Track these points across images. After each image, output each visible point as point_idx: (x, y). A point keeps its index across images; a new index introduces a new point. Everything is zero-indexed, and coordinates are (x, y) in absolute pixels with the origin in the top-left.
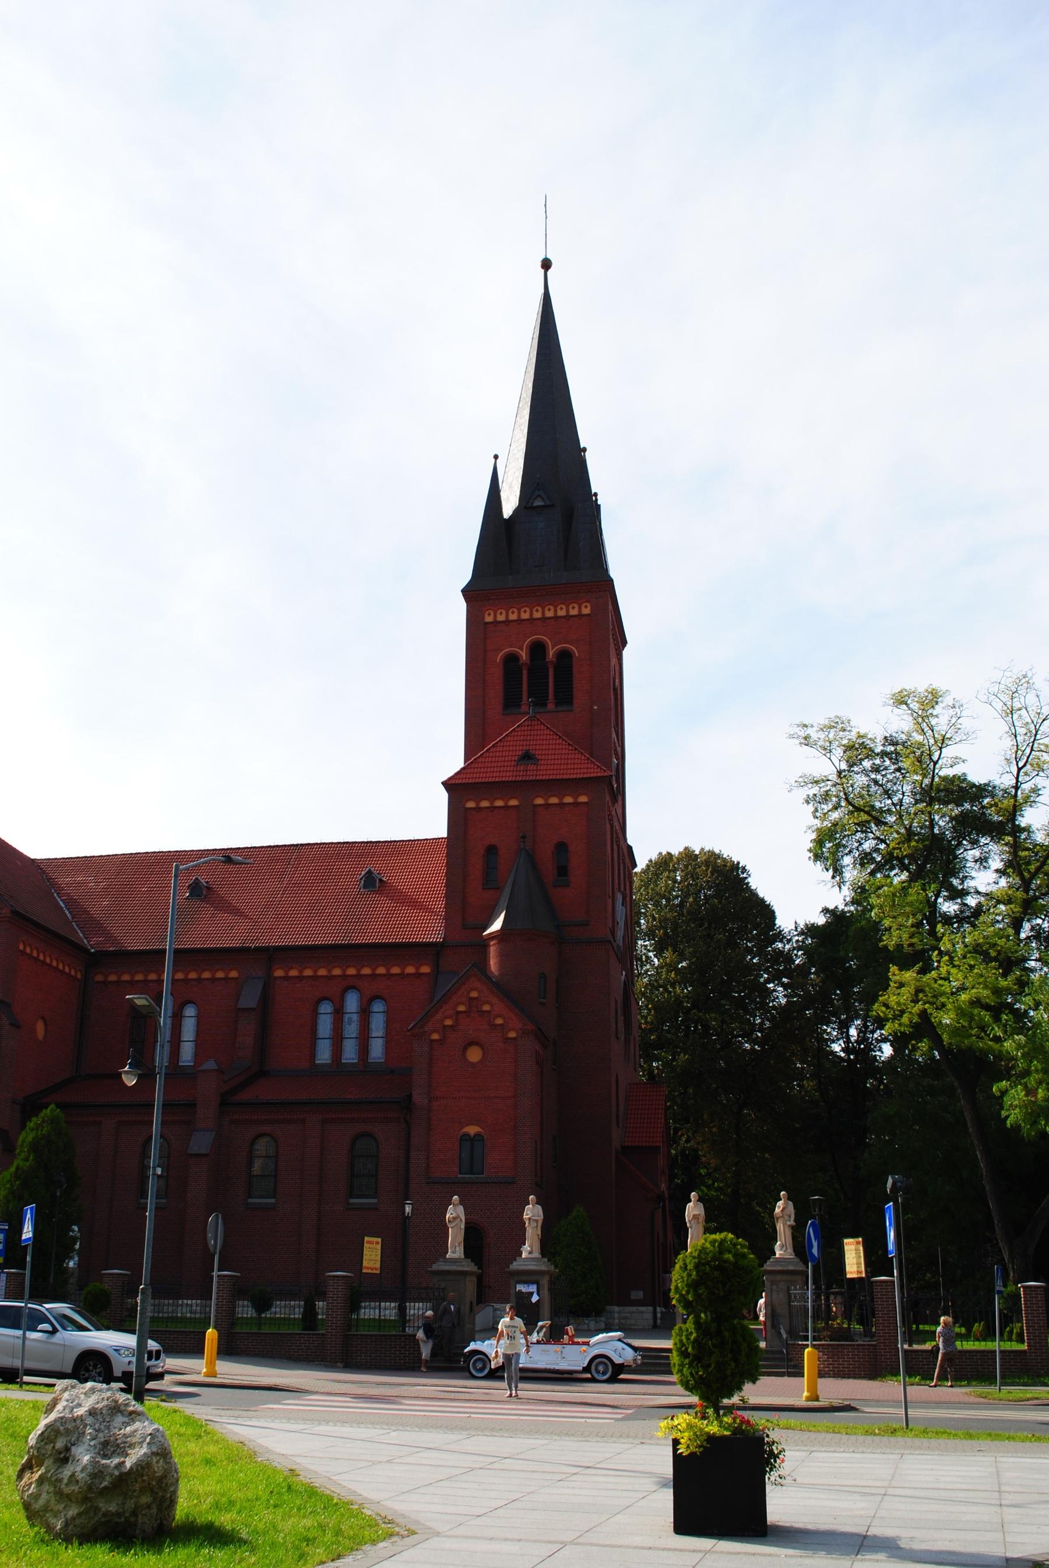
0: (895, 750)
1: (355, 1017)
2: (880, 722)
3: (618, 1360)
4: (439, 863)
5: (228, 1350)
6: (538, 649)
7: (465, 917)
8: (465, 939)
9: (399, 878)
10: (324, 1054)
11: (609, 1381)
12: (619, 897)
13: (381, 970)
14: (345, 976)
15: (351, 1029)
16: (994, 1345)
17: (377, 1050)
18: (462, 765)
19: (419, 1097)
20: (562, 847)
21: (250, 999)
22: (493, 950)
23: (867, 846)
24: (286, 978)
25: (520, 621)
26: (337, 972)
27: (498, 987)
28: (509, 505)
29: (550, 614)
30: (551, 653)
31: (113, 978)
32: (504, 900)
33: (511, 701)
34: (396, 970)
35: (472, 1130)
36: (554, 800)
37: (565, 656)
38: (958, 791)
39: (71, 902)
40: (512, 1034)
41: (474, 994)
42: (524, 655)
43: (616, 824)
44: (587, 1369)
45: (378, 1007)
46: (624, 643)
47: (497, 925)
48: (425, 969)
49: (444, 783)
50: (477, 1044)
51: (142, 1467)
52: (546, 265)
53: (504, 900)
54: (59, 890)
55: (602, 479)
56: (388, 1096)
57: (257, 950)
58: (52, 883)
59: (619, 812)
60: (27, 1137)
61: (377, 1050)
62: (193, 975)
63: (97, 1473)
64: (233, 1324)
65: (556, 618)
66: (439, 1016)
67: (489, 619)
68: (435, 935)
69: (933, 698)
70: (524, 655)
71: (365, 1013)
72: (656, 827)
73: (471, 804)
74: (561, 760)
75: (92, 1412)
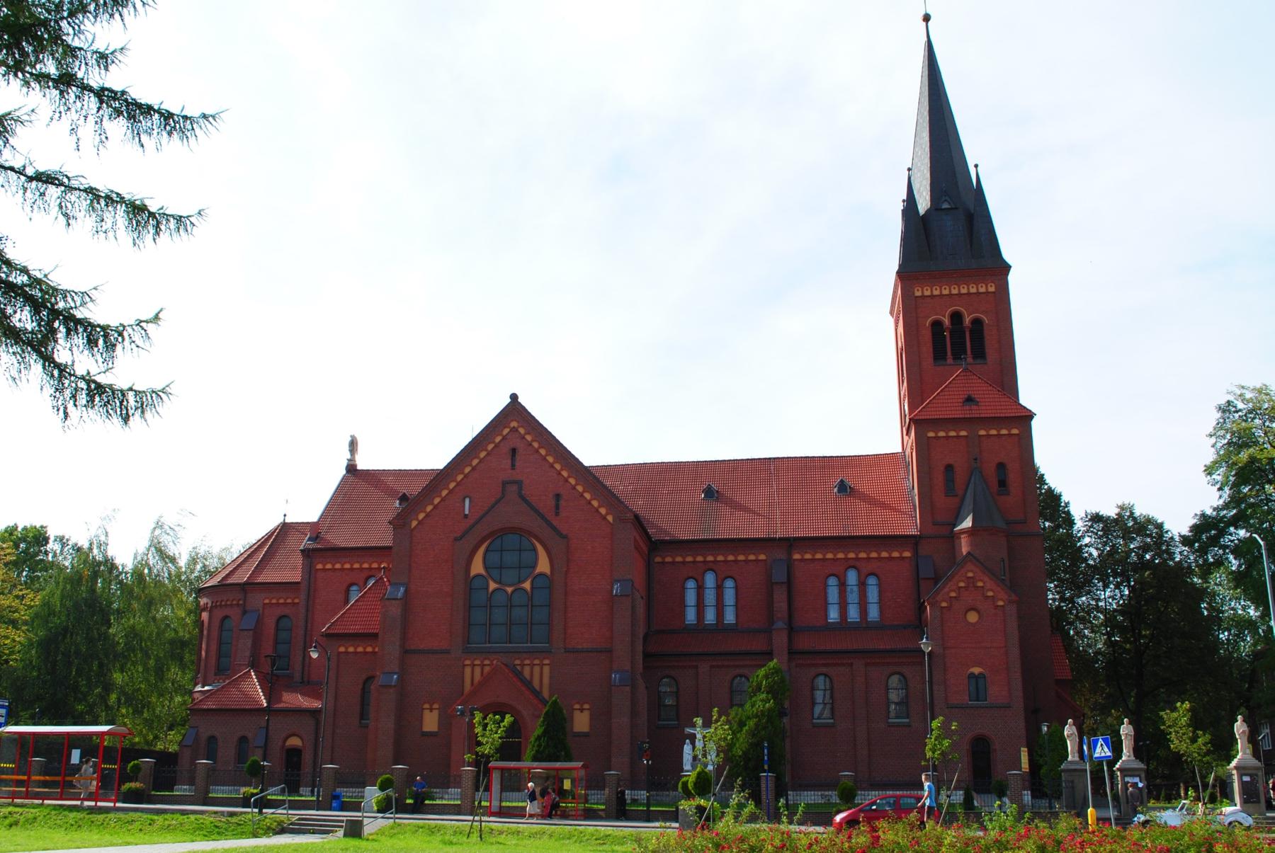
1: (855, 589)
6: (956, 317)
13: (874, 555)
14: (847, 559)
17: (730, 617)
20: (1001, 466)
21: (780, 575)
24: (802, 560)
25: (941, 295)
26: (841, 556)
28: (923, 204)
29: (964, 291)
30: (967, 320)
31: (669, 559)
33: (939, 355)
35: (976, 670)
36: (994, 432)
37: (977, 322)
40: (1001, 603)
41: (970, 575)
42: (946, 321)
47: (967, 523)
48: (907, 554)
49: (514, 411)
52: (927, 18)
57: (780, 539)
61: (874, 613)
65: (969, 294)
66: (946, 590)
67: (918, 294)
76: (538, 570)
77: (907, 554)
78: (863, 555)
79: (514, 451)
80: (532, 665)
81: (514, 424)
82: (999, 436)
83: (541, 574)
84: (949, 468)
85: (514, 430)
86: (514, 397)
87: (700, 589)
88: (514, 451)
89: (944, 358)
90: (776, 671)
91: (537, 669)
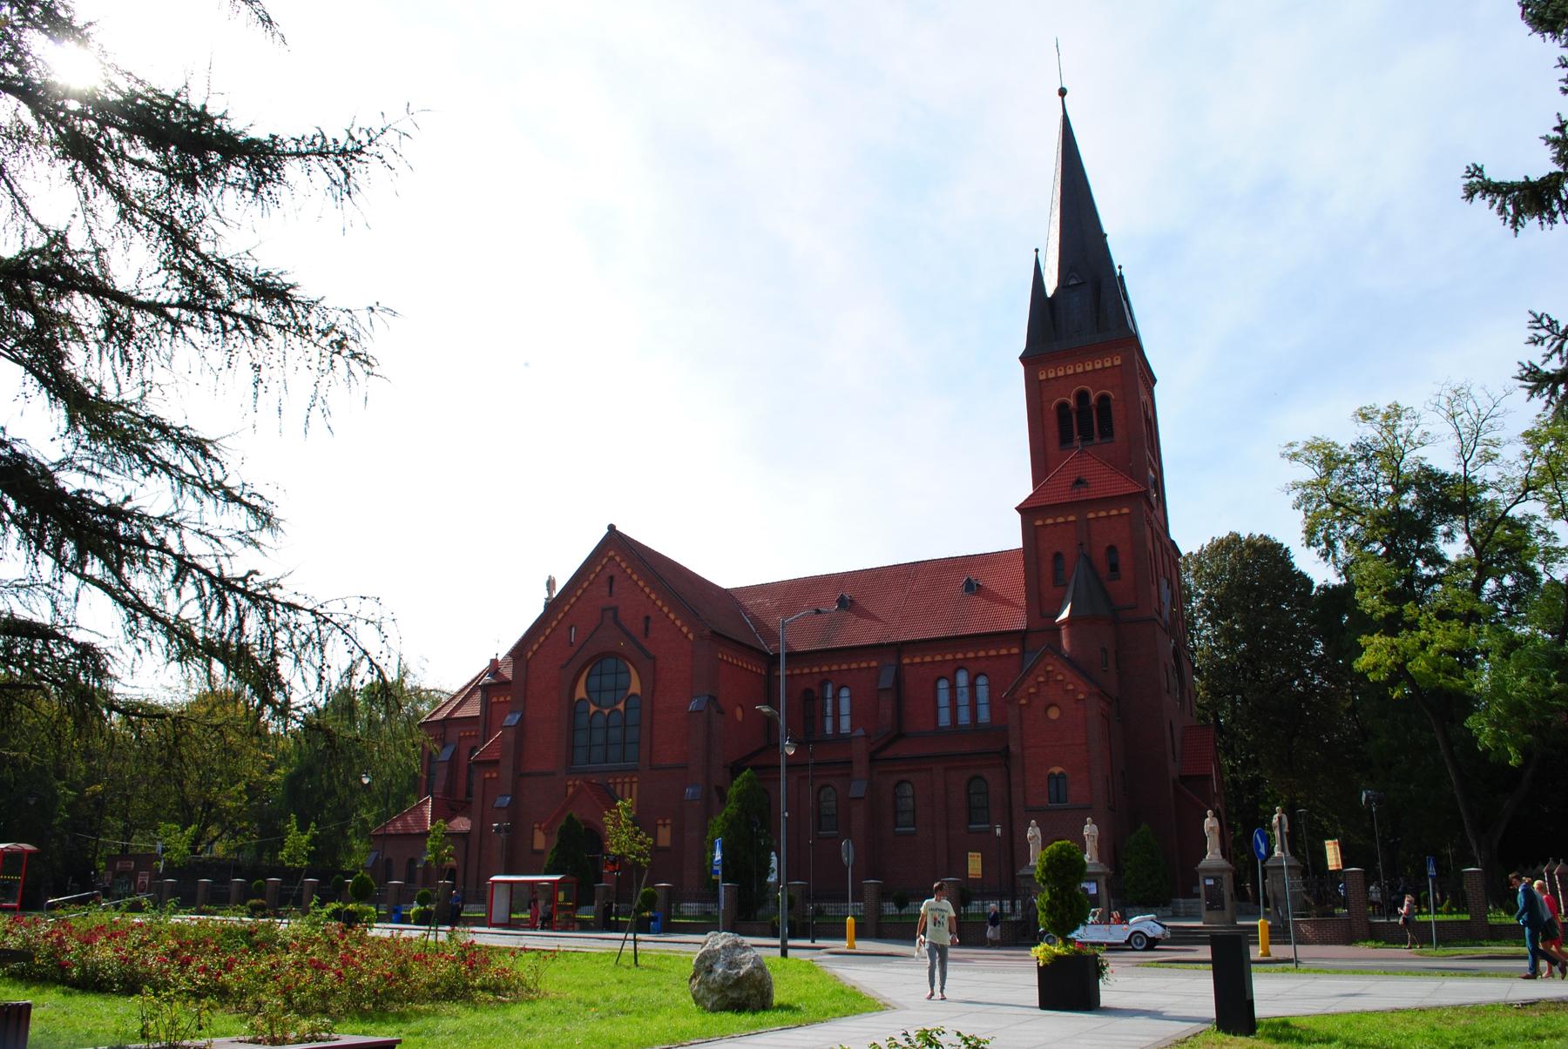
0: (1366, 453)
2: (1346, 435)
3: (1150, 935)
4: (1019, 567)
5: (861, 934)
6: (1082, 396)
7: (1041, 608)
8: (1041, 630)
9: (991, 582)
10: (944, 719)
11: (1145, 950)
12: (1164, 583)
13: (982, 654)
14: (955, 660)
15: (963, 699)
16: (1431, 918)
17: (984, 715)
18: (1031, 491)
19: (1014, 748)
20: (1112, 549)
21: (886, 681)
22: (1064, 633)
23: (1351, 531)
24: (911, 664)
26: (949, 657)
27: (1071, 662)
28: (1051, 285)
30: (1093, 399)
32: (1070, 595)
33: (1065, 439)
34: (993, 653)
35: (1056, 770)
37: (1104, 399)
38: (1428, 478)
39: (754, 619)
40: (1081, 696)
42: (1072, 402)
43: (1156, 525)
44: (1128, 942)
45: (982, 681)
46: (1154, 381)
47: (1065, 614)
48: (1015, 651)
49: (614, 541)
50: (1051, 705)
51: (749, 974)
52: (1063, 92)
53: (1070, 595)
54: (745, 610)
55: (1120, 254)
56: (990, 749)
57: (890, 644)
58: (740, 606)
59: (1160, 514)
60: (732, 791)
61: (984, 715)
62: (844, 667)
63: (726, 977)
64: (880, 917)
67: (1042, 377)
68: (1021, 625)
69: (1395, 412)
70: (1072, 402)
71: (972, 685)
72: (1193, 525)
73: (1039, 523)
74: (1105, 482)
75: (724, 947)
76: (631, 691)
77: (1015, 651)
78: (971, 655)
79: (611, 578)
80: (623, 783)
81: (611, 553)
82: (1109, 517)
83: (634, 695)
84: (1058, 556)
85: (612, 559)
86: (612, 528)
87: (953, 687)
88: (611, 578)
89: (1071, 440)
90: (749, 779)
91: (627, 787)
